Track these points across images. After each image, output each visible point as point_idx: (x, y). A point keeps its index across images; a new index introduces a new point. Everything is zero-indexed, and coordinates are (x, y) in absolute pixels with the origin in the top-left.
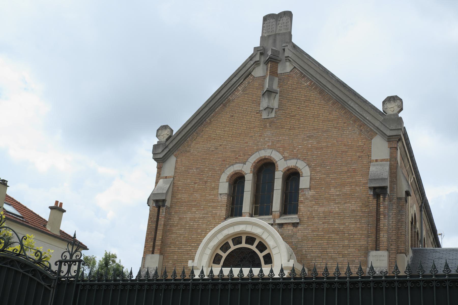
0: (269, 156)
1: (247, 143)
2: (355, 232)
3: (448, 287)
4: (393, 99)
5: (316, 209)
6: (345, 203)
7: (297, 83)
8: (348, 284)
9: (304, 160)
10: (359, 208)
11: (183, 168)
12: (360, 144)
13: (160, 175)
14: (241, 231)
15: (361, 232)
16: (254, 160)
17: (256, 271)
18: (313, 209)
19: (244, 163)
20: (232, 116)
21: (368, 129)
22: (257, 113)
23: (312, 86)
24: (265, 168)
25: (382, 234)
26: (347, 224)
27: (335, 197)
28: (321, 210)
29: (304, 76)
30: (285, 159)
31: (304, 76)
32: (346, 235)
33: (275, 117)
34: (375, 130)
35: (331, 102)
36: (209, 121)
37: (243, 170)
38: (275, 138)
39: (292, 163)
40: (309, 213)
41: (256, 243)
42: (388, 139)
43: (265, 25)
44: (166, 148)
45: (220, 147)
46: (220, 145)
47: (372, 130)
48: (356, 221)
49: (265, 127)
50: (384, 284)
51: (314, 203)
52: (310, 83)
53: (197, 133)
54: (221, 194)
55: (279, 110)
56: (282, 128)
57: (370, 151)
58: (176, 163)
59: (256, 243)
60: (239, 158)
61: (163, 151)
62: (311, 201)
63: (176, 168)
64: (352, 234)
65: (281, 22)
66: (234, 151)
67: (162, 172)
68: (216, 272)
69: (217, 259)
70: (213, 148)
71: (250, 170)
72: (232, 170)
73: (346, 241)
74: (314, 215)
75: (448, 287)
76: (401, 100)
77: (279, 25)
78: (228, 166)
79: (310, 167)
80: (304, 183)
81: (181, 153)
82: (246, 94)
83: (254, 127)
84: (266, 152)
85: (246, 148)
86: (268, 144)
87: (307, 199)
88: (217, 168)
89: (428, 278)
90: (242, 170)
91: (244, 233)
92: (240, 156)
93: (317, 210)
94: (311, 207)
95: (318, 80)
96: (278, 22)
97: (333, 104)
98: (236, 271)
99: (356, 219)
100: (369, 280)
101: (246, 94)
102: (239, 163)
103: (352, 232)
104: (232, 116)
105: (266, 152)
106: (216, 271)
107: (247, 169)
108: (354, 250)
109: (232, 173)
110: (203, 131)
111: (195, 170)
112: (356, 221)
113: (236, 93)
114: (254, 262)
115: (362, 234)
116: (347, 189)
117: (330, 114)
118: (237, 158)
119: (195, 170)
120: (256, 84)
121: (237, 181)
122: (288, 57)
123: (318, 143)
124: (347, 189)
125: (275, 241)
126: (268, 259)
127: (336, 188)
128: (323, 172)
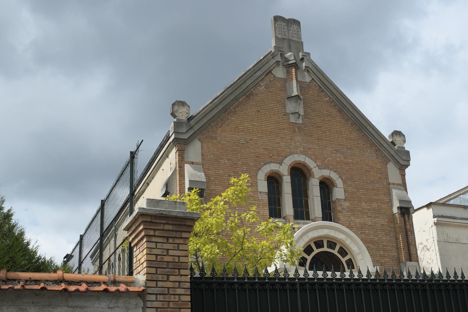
0: (303, 162)
1: (278, 143)
2: (387, 244)
3: (308, 290)
4: (397, 133)
5: (353, 219)
6: (376, 217)
7: (318, 96)
8: (298, 286)
9: (335, 171)
10: (386, 223)
11: (212, 156)
12: (378, 166)
13: (183, 158)
14: (325, 235)
15: (391, 244)
16: (290, 163)
17: (338, 274)
18: (350, 219)
19: (281, 164)
20: (259, 111)
21: (383, 155)
22: (284, 115)
23: (331, 102)
24: (299, 174)
25: (412, 248)
26: (380, 236)
27: (367, 211)
28: (357, 221)
29: (323, 91)
30: (320, 167)
31: (323, 91)
32: (381, 246)
33: (303, 124)
34: (389, 157)
35: (350, 122)
36: (233, 110)
37: (280, 170)
38: (305, 145)
39: (326, 173)
40: (348, 222)
41: (314, 247)
42: (400, 167)
43: (276, 25)
44: (190, 129)
45: (251, 141)
46: (251, 140)
47: (385, 156)
48: (386, 235)
49: (294, 131)
50: (247, 286)
51: (350, 213)
52: (330, 99)
53: (222, 120)
54: (260, 192)
55: (305, 117)
56: (311, 136)
57: (387, 175)
58: (202, 148)
59: (314, 247)
60: (273, 157)
61: (187, 131)
62: (348, 212)
63: (202, 155)
64: (385, 246)
65: (292, 28)
66: (267, 149)
67: (185, 156)
68: (301, 273)
69: (302, 263)
70: (242, 141)
71: (287, 172)
72: (269, 169)
73: (381, 251)
74: (352, 225)
75: (308, 290)
76: (404, 136)
77: (291, 31)
78: (263, 164)
79: (342, 179)
80: (338, 193)
81: (206, 138)
82: (270, 92)
83: (284, 129)
84: (300, 156)
85: (279, 149)
86: (300, 149)
87: (344, 209)
88: (252, 164)
89: (220, 281)
90: (278, 171)
91: (325, 237)
92: (273, 155)
93: (354, 221)
94: (349, 217)
95: (338, 99)
96: (289, 28)
97: (352, 125)
98: (320, 274)
100: (211, 281)
101: (270, 92)
102: (274, 162)
103: (385, 244)
104: (259, 111)
105: (300, 156)
106: (301, 273)
107: (284, 170)
108: (389, 260)
109: (269, 171)
110: (228, 119)
111: (226, 161)
112: (386, 235)
113: (259, 88)
114: (338, 266)
115: (392, 246)
116: (375, 205)
117: (350, 133)
118: (270, 157)
119: (226, 161)
120: (279, 85)
121: (274, 181)
122: (308, 67)
123: (345, 158)
124: (375, 205)
125: (359, 248)
126: (351, 264)
127: (366, 202)
128: (354, 186)
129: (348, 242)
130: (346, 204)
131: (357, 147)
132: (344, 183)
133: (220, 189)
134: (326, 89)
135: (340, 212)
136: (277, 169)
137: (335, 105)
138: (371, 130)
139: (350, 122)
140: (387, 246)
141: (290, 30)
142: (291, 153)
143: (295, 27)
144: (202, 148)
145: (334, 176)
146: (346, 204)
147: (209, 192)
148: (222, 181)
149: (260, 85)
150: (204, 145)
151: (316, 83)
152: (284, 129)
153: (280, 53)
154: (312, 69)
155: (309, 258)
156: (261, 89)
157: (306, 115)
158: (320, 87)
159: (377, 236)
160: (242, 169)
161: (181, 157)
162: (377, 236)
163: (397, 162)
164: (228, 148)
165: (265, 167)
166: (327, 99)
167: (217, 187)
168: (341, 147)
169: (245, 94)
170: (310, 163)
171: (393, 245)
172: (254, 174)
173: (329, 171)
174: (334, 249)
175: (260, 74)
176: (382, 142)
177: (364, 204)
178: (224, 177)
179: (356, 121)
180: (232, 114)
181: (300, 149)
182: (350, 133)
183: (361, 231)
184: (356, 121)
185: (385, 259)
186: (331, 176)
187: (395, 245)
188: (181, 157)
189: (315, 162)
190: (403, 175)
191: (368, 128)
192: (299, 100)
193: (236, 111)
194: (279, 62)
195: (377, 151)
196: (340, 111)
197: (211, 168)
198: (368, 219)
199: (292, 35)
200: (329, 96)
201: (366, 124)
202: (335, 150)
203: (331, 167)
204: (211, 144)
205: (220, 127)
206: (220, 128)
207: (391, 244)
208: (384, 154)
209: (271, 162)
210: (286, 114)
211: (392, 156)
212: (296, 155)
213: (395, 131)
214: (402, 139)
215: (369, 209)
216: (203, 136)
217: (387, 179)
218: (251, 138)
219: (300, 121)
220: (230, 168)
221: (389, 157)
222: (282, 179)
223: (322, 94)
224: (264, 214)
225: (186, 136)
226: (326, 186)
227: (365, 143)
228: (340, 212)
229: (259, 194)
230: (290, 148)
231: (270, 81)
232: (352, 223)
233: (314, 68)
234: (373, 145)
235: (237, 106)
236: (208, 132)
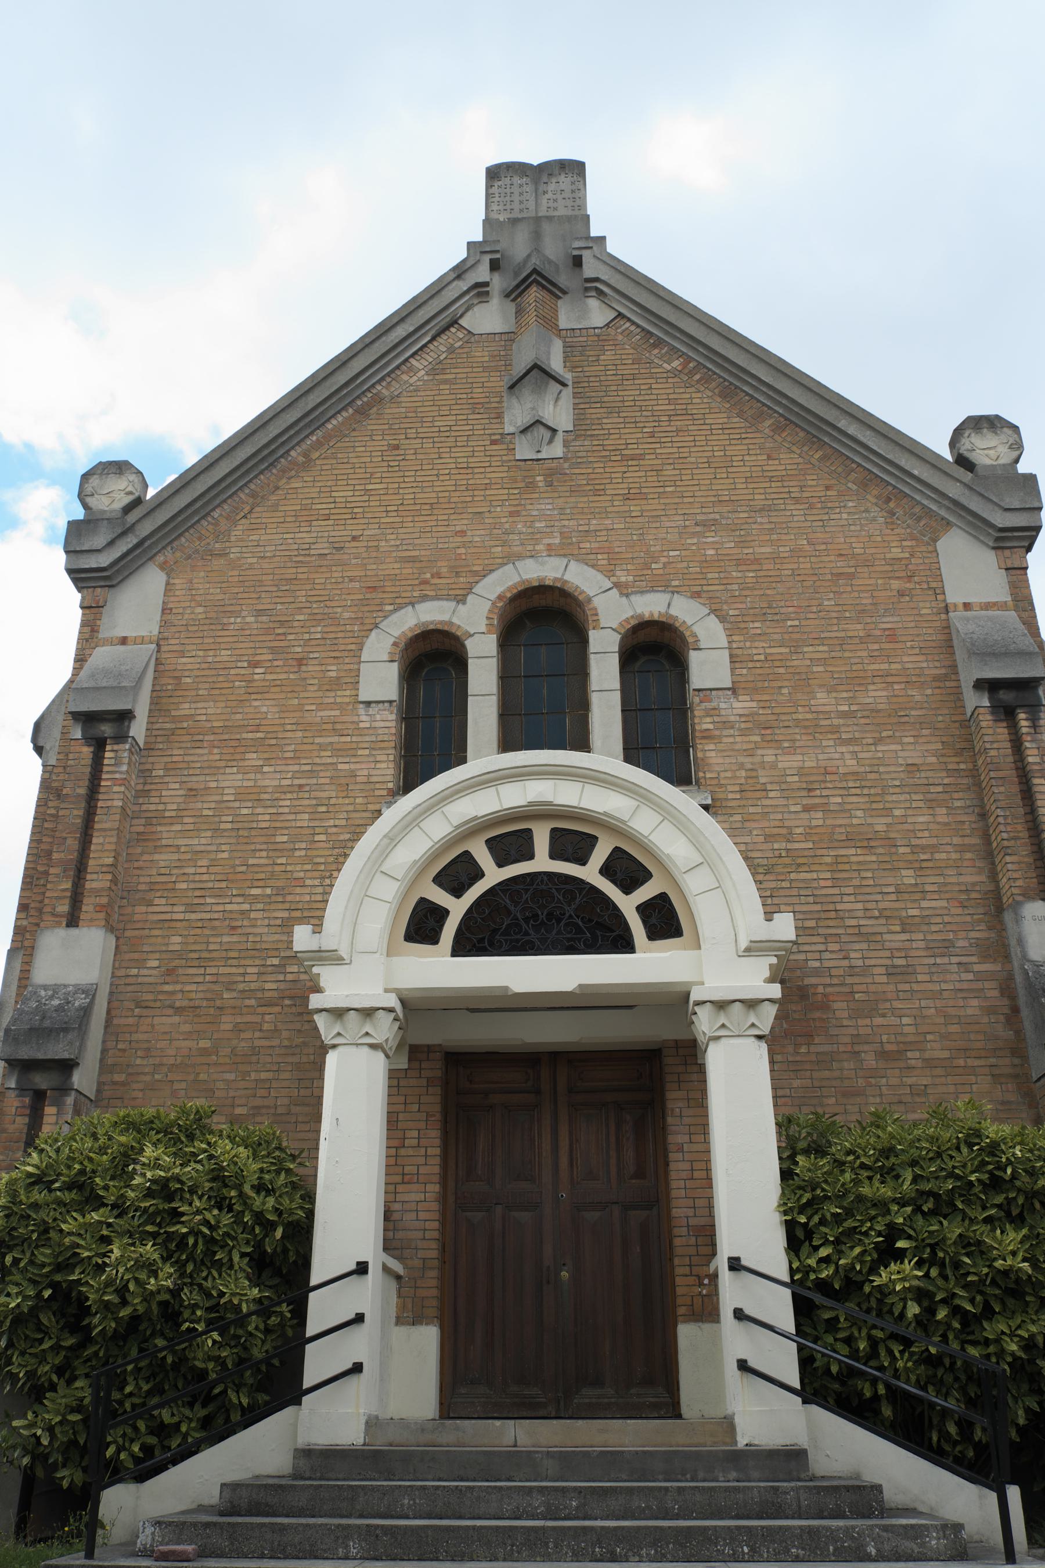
1: (462, 533)
2: (934, 841)
10: (933, 760)
11: (200, 610)
12: (896, 552)
14: (531, 804)
15: (956, 840)
16: (499, 590)
18: (757, 759)
20: (397, 447)
22: (494, 442)
23: (691, 373)
24: (544, 622)
26: (897, 812)
27: (836, 722)
28: (789, 762)
29: (659, 343)
30: (624, 590)
32: (901, 850)
33: (565, 458)
34: (943, 513)
36: (301, 459)
38: (572, 523)
39: (651, 605)
40: (743, 773)
43: (495, 190)
44: (124, 534)
46: (354, 538)
47: (929, 513)
49: (531, 486)
51: (757, 738)
52: (685, 365)
54: (368, 703)
56: (596, 493)
57: (939, 578)
61: (111, 543)
62: (744, 732)
63: (165, 610)
64: (923, 848)
65: (552, 187)
66: (413, 560)
70: (322, 547)
73: (904, 872)
74: (763, 780)
76: (1015, 429)
78: (391, 608)
79: (722, 619)
80: (708, 668)
81: (189, 557)
82: (445, 382)
83: (487, 487)
87: (726, 724)
88: (346, 615)
90: (451, 623)
93: (774, 766)
96: (542, 187)
97: (777, 429)
99: (929, 796)
101: (445, 382)
102: (437, 598)
103: (924, 842)
108: (944, 903)
109: (411, 629)
110: (277, 488)
112: (931, 804)
113: (405, 377)
114: (597, 929)
117: (769, 458)
118: (425, 582)
120: (481, 355)
123: (741, 543)
126: (664, 920)
129: (644, 823)
130: (736, 705)
131: (797, 500)
132: (733, 627)
133: (209, 711)
134: (667, 333)
135: (708, 736)
136: (446, 617)
137: (706, 380)
138: (852, 429)
139: (768, 423)
140: (934, 848)
141: (545, 193)
142: (510, 558)
143: (565, 181)
144: (169, 587)
145: (685, 611)
146: (742, 705)
147: (168, 726)
148: (226, 685)
149: (411, 369)
150: (176, 581)
151: (633, 323)
152: (487, 487)
153: (487, 259)
154: (612, 282)
155: (457, 908)
156: (412, 381)
157: (581, 428)
158: (649, 332)
159: (887, 812)
160: (307, 636)
161: (87, 629)
162: (887, 812)
163: (977, 524)
164: (264, 578)
165: (395, 617)
166: (676, 364)
167: (199, 705)
168: (725, 509)
169: (350, 404)
170: (582, 579)
171: (967, 840)
172: (353, 647)
173: (665, 598)
174: (531, 856)
175: (404, 334)
176: (905, 461)
177: (821, 697)
178: (233, 672)
179: (791, 410)
180: (293, 473)
181: (547, 541)
182: (769, 458)
183: (805, 802)
184: (791, 410)
185: (924, 904)
186: (673, 612)
187: (975, 840)
188: (87, 629)
189: (609, 573)
190: (1018, 573)
191: (842, 424)
192: (554, 387)
193: (311, 460)
194: (486, 284)
195: (888, 500)
196: (727, 393)
197: (188, 648)
198: (844, 749)
199: (551, 204)
200: (684, 353)
201: (830, 414)
202: (696, 524)
203: (675, 583)
204: (202, 574)
205: (245, 517)
206: (243, 521)
207: (956, 840)
208: (924, 506)
209: (424, 598)
210: (501, 439)
211: (956, 503)
212: (529, 562)
213: (969, 419)
214: (1003, 438)
215: (844, 715)
216: (178, 554)
217: (938, 591)
218: (354, 533)
219: (557, 450)
220: (263, 638)
221: (943, 513)
222: (464, 646)
223: (656, 351)
224: (374, 779)
225: (104, 560)
226: (656, 651)
227: (833, 482)
228: (708, 736)
229: (362, 712)
230: (504, 544)
231: (451, 350)
232: (761, 772)
233: (618, 276)
234: (868, 481)
235: (319, 444)
236: (200, 539)
